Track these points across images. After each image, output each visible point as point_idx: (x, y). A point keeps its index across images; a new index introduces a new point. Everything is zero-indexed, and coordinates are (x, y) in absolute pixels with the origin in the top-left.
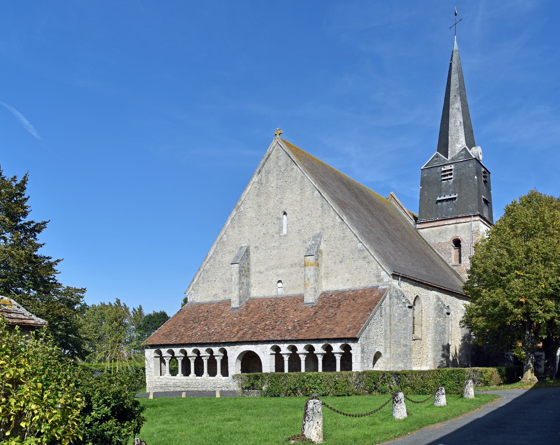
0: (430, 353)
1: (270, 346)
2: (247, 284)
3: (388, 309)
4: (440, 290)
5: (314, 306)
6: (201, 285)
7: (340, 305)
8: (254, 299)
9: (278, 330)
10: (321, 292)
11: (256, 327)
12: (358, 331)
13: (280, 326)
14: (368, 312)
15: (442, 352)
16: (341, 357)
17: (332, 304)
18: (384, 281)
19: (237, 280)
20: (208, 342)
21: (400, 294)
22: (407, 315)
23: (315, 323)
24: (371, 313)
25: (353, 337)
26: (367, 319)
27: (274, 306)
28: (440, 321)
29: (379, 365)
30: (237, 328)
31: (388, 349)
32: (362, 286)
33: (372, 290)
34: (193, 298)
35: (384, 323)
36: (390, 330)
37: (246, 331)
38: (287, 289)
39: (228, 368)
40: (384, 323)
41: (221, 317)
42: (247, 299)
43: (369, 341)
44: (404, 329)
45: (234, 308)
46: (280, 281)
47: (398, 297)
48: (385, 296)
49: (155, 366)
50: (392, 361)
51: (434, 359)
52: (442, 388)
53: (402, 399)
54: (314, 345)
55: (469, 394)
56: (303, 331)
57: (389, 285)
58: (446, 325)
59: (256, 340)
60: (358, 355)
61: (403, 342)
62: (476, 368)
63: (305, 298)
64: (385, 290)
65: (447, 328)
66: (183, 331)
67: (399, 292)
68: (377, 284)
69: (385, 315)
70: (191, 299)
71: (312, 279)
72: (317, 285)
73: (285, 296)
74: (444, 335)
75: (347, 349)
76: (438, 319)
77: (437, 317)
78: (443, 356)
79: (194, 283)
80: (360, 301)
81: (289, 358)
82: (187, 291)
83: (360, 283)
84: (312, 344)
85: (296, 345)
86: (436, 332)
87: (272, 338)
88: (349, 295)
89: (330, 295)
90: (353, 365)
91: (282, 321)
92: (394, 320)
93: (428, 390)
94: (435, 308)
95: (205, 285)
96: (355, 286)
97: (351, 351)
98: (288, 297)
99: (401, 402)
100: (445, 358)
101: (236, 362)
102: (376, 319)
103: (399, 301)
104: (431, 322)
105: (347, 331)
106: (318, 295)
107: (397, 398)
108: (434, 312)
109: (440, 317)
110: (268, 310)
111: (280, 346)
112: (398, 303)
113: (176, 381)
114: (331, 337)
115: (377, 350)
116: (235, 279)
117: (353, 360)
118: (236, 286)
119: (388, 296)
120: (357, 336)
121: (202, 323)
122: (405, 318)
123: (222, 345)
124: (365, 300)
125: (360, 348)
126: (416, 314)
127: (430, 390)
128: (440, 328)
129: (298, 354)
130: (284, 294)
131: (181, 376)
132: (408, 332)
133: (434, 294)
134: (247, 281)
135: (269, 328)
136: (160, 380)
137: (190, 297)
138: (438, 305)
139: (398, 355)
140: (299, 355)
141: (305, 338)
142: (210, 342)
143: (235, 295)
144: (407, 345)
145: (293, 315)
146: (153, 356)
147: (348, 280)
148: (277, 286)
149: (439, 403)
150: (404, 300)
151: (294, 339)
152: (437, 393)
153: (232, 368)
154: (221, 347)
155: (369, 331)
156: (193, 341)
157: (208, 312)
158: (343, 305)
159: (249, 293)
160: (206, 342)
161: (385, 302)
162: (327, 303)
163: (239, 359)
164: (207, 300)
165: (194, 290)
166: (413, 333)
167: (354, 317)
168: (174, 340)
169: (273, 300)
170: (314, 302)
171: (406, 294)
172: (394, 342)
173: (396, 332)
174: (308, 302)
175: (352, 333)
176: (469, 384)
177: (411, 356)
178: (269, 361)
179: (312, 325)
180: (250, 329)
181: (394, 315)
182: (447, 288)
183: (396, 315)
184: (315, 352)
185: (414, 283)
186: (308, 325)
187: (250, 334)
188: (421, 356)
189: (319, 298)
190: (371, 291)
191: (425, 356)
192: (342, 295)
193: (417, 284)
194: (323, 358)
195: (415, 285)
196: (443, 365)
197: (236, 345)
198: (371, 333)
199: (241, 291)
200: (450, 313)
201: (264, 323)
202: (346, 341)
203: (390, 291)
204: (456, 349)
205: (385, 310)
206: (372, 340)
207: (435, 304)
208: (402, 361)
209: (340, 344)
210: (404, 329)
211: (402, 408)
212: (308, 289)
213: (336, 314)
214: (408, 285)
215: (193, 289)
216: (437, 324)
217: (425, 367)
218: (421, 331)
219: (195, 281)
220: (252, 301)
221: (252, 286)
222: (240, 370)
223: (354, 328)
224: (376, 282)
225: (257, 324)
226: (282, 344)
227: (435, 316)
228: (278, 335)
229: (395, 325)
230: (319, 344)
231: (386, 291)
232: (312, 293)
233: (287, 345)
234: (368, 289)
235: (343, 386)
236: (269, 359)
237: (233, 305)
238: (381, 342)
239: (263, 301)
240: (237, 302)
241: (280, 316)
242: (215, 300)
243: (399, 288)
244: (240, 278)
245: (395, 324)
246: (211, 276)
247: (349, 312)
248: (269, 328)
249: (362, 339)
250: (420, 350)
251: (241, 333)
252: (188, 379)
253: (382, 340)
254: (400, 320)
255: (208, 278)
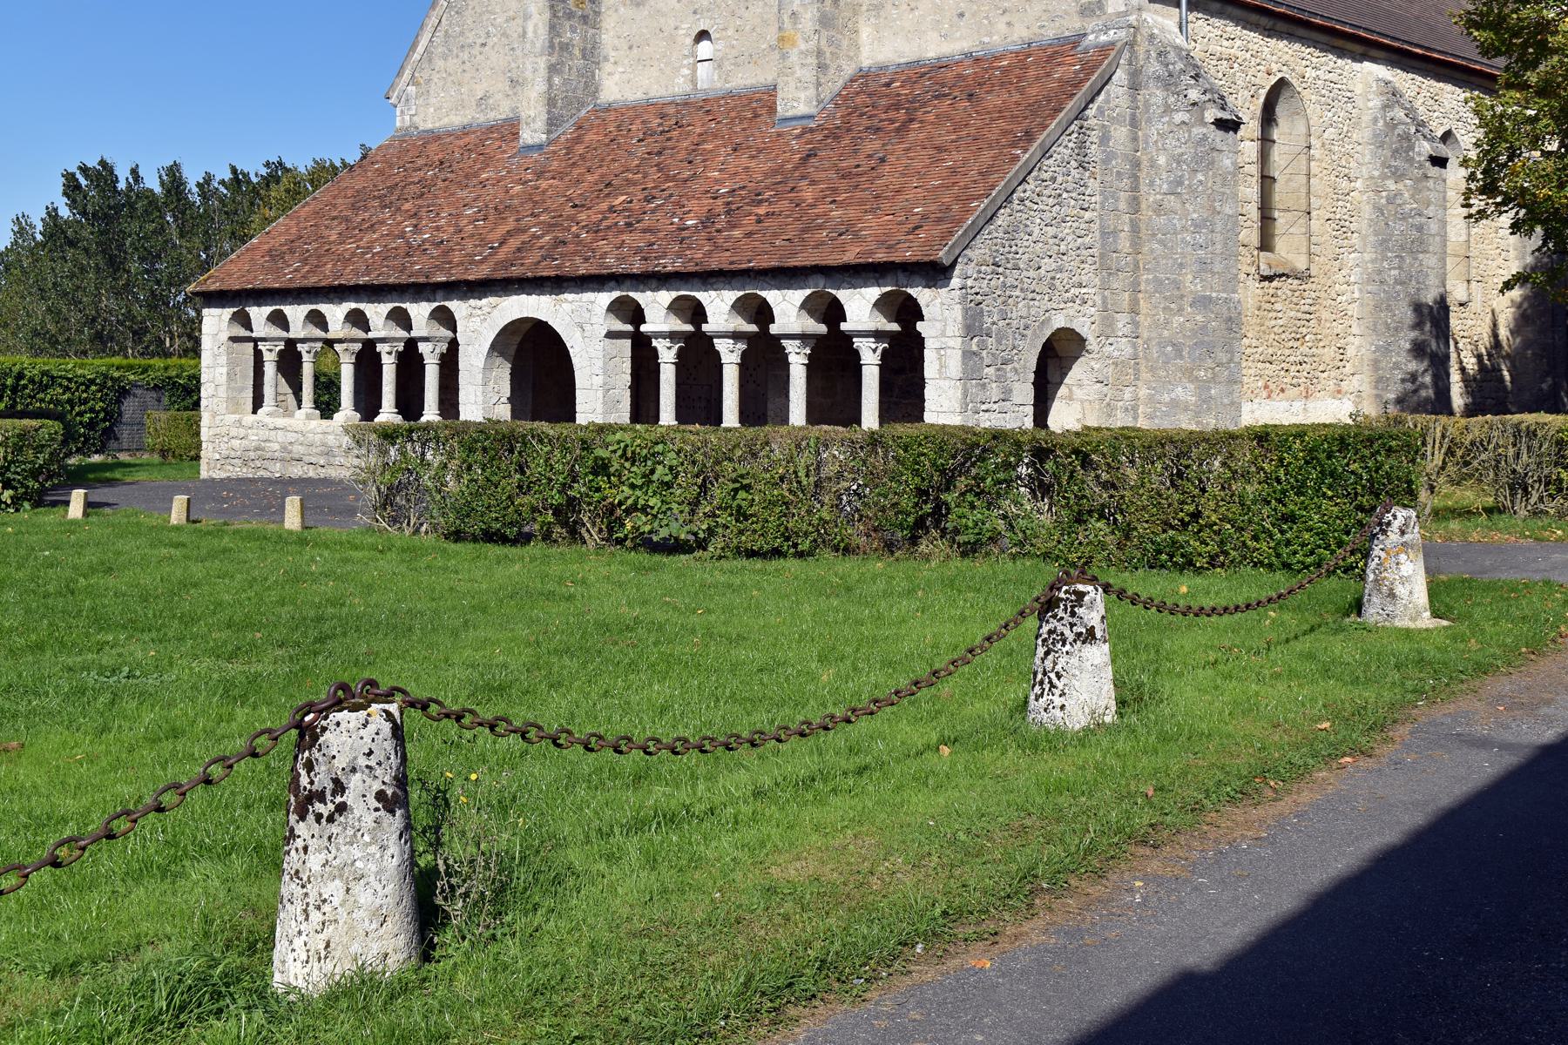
0: (1357, 341)
1: (605, 298)
2: (583, 50)
3: (1120, 133)
4: (1405, 60)
5: (812, 130)
6: (439, 64)
7: (911, 120)
8: (608, 109)
9: (644, 231)
10: (849, 70)
11: (572, 218)
12: (951, 233)
13: (659, 215)
14: (1013, 145)
15: (1413, 334)
16: (885, 353)
17: (884, 116)
18: (1110, 10)
19: (543, 32)
20: (391, 280)
21: (1180, 66)
22: (1213, 163)
23: (791, 201)
24: (1026, 151)
25: (926, 259)
26: (1002, 178)
27: (668, 135)
28: (1399, 194)
29: (1078, 393)
30: (511, 224)
31: (1122, 322)
32: (1015, 37)
33: (1056, 52)
34: (413, 112)
35: (1097, 198)
36: (1135, 229)
37: (534, 237)
38: (727, 66)
39: (457, 390)
40: (1097, 198)
41: (475, 181)
42: (583, 112)
43: (1010, 281)
44: (1196, 226)
45: (530, 148)
46: (703, 35)
47: (1169, 82)
48: (1101, 76)
49: (231, 376)
50: (1145, 375)
51: (1375, 364)
52: (1081, 595)
53: (355, 783)
54: (772, 296)
55: (1392, 595)
56: (737, 233)
57: (1130, 26)
58: (1430, 211)
59: (553, 274)
60: (951, 343)
61: (1192, 285)
62: (1529, 419)
63: (780, 95)
64: (1105, 49)
65: (1434, 227)
66: (333, 238)
67: (1172, 56)
68: (1078, 25)
69: (1106, 161)
70: (407, 118)
71: (809, 16)
72: (830, 42)
73: (720, 93)
74: (1421, 256)
75: (908, 312)
76: (1391, 185)
77: (1384, 177)
78: (1418, 350)
79: (416, 56)
80: (993, 100)
81: (744, 355)
82: (392, 87)
83: (1009, 24)
84: (763, 294)
85: (701, 296)
86: (1383, 244)
87: (612, 264)
88: (960, 77)
89: (884, 80)
90: (929, 393)
91: (671, 195)
92: (1152, 183)
93: (1204, 543)
94: (1375, 136)
95: (452, 64)
96: (986, 40)
97: (920, 326)
98: (730, 95)
99: (342, 808)
100: (1426, 363)
101: (487, 368)
102: (1054, 179)
103: (1172, 99)
104: (1361, 198)
105: (908, 233)
106: (834, 84)
107: (309, 766)
108: (1374, 155)
109: (1398, 176)
110: (641, 150)
111: (643, 298)
112: (1168, 110)
113: (291, 437)
114: (834, 259)
115: (1059, 322)
116: (535, 32)
117: (930, 370)
118: (539, 60)
119: (1120, 76)
120: (941, 254)
121: (407, 206)
122: (1200, 177)
123: (440, 294)
124: (1016, 97)
125: (957, 313)
126: (1283, 163)
127: (1213, 547)
128: (1398, 227)
129: (711, 338)
130: (719, 85)
131: (309, 417)
132: (1218, 238)
133: (1370, 73)
134: (584, 39)
135: (616, 224)
136: (242, 432)
137: (402, 112)
138: (1392, 125)
139: (1169, 348)
140: (715, 341)
141: (732, 267)
142: (397, 281)
143: (533, 94)
144: (1210, 298)
145: (720, 170)
146: (224, 336)
147: (961, 15)
148: (694, 55)
149: (1058, 701)
150: (1194, 95)
151: (691, 268)
152: (1045, 629)
153: (471, 389)
154: (437, 304)
155: (1011, 232)
156: (348, 279)
157: (442, 163)
158: (921, 122)
159: (592, 87)
160: (384, 282)
161: (1107, 101)
162: (864, 114)
163: (502, 354)
164: (456, 120)
165: (417, 84)
166: (1266, 244)
167: (953, 171)
168: (290, 273)
169: (671, 110)
170: (814, 111)
171: (1210, 68)
172: (1150, 288)
173: (1161, 242)
174: (790, 114)
175: (928, 242)
176: (1393, 536)
177: (1231, 352)
178: (600, 363)
179: (776, 208)
180: (549, 227)
181: (1153, 164)
182: (1439, 52)
183: (1162, 160)
184: (774, 329)
185: (1264, 21)
186: (762, 211)
187: (541, 248)
188: (1305, 349)
189: (839, 94)
190: (1051, 58)
191: (1329, 353)
192: (929, 79)
193: (1281, 26)
194: (810, 357)
195: (1269, 32)
196: (1415, 391)
197: (486, 297)
198: (1024, 241)
199: (556, 80)
200: (1446, 160)
201: (604, 206)
202: (902, 277)
203: (1133, 52)
204: (1495, 325)
205: (1105, 139)
206: (1032, 274)
207: (1375, 120)
208: (1189, 374)
209: (873, 293)
210: (1198, 226)
211: (340, 873)
212: (794, 57)
213: (882, 160)
214: (1232, 29)
215: (413, 81)
216: (1388, 210)
217: (1330, 401)
218: (1304, 239)
219: (420, 49)
220: (597, 118)
221: (606, 59)
222: (504, 400)
223: (939, 221)
224: (1076, 18)
225: (583, 206)
226: (649, 293)
227: (1376, 173)
228: (638, 251)
229: (1159, 208)
230: (789, 293)
231: (1113, 53)
232: (808, 74)
233: (666, 297)
234: (1042, 49)
235: (773, 503)
236: (600, 354)
237: (532, 135)
238: (1080, 285)
239: (637, 117)
240: (540, 124)
241: (675, 176)
242: (481, 118)
243: (1180, 40)
244: (552, 27)
245: (1155, 202)
246: (472, 26)
247: (939, 149)
248: (616, 224)
249: (971, 269)
250: (1299, 323)
251: (514, 243)
252: (330, 430)
253: (1088, 274)
254: (1180, 183)
255: (462, 33)
